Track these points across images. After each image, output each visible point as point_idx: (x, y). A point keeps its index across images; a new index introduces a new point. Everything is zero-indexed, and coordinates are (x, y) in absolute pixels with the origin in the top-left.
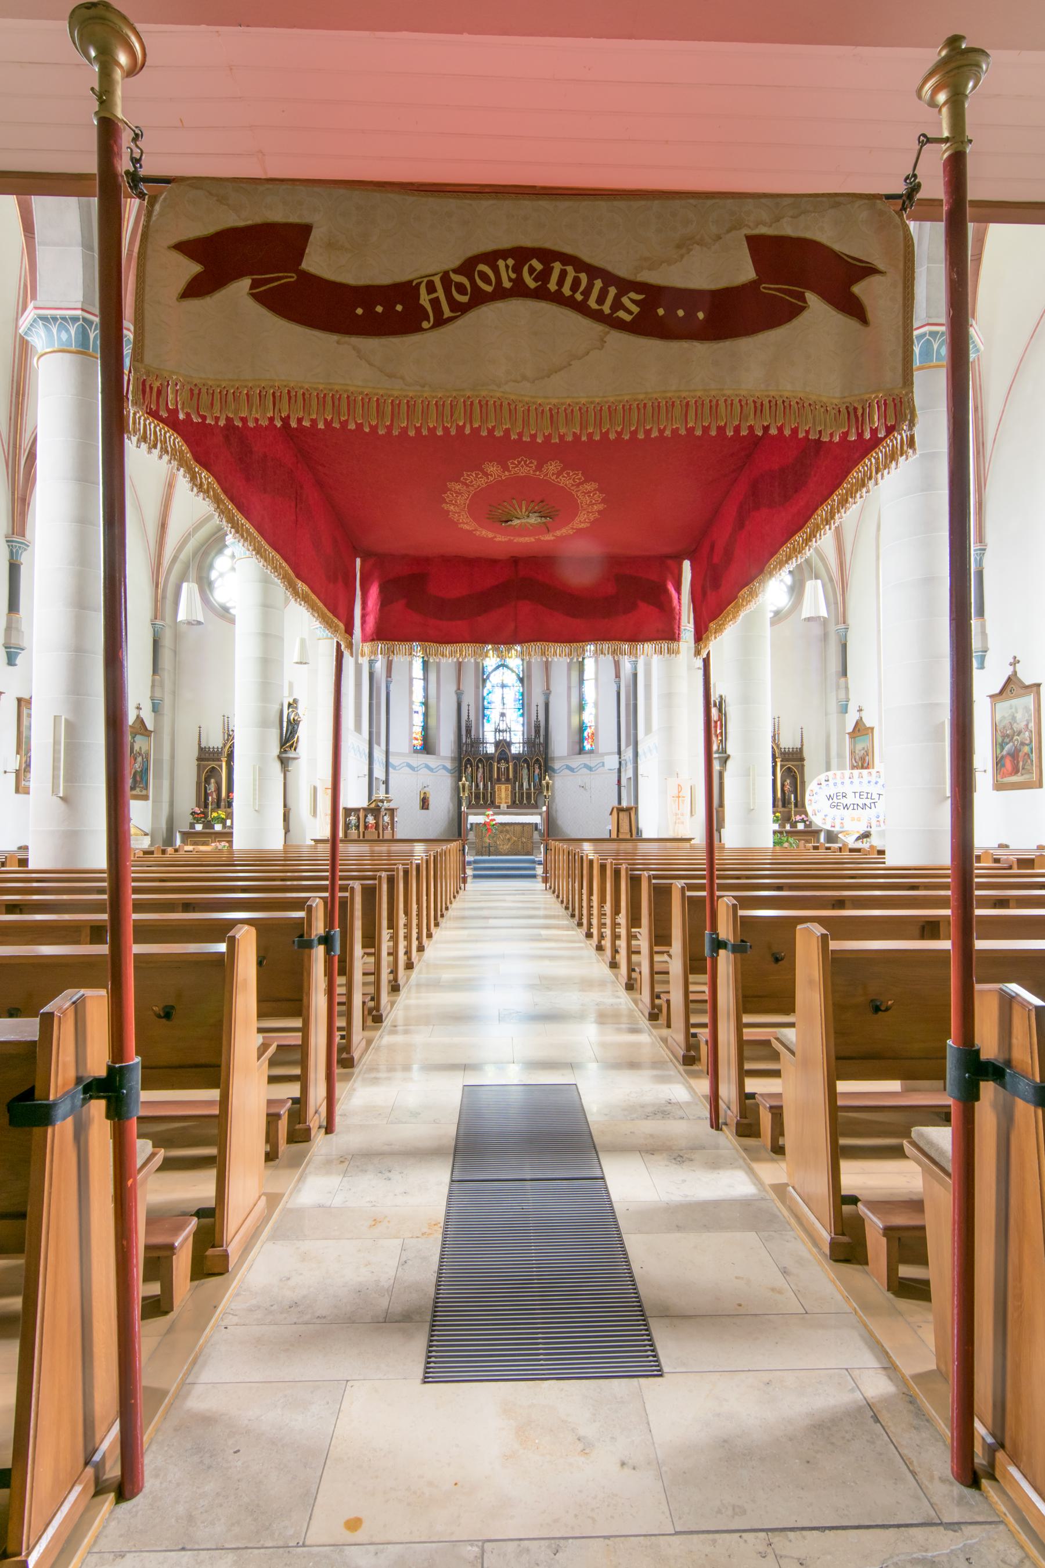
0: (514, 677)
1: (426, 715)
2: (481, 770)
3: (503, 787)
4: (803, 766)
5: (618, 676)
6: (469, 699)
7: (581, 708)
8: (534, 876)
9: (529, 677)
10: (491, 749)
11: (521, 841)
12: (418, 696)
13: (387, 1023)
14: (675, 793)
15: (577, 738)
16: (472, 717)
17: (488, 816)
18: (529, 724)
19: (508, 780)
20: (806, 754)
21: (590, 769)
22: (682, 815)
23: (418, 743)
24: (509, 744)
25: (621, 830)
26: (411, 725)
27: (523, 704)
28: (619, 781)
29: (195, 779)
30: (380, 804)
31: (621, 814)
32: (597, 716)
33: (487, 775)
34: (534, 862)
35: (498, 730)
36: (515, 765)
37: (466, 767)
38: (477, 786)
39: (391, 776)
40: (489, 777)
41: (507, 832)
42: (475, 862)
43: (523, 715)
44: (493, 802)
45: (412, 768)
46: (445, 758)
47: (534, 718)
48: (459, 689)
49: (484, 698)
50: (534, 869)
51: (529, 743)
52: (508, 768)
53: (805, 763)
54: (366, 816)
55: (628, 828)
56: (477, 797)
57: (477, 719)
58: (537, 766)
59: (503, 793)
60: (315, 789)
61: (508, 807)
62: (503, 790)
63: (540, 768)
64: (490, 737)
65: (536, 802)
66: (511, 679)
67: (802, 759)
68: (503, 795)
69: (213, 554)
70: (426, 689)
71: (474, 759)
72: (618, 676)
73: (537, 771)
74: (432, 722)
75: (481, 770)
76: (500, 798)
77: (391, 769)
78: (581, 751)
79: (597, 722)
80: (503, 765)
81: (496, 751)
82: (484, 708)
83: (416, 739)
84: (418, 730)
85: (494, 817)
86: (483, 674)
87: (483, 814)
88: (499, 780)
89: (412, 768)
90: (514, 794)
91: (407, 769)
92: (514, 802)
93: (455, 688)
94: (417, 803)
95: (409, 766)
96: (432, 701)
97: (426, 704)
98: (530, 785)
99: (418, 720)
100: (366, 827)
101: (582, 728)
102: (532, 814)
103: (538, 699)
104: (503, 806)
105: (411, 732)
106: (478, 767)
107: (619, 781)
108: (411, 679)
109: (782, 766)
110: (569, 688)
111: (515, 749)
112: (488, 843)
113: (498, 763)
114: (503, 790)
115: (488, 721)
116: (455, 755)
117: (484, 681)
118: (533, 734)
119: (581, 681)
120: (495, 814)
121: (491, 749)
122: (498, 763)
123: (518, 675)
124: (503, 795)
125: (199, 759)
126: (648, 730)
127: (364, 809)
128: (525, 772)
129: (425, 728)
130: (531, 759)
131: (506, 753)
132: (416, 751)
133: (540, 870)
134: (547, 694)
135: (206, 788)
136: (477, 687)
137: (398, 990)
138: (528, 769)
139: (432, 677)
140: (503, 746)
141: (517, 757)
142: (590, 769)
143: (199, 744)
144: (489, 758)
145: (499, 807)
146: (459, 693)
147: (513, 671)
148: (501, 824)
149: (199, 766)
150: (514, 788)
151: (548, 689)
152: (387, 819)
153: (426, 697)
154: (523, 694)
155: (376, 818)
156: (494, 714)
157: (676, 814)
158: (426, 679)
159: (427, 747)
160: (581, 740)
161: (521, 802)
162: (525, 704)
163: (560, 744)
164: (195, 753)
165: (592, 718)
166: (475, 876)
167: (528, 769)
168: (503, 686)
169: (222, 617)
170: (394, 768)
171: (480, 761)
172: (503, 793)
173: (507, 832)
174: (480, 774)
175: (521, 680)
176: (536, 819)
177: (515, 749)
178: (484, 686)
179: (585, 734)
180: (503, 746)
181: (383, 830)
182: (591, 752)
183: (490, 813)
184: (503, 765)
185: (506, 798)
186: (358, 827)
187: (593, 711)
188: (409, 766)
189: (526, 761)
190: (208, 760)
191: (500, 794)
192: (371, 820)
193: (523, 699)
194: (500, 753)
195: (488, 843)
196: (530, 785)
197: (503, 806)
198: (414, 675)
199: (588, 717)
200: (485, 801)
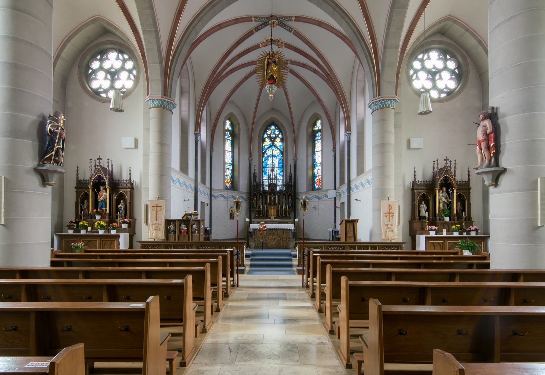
0: (278, 151)
1: (233, 170)
2: (261, 199)
3: (272, 207)
4: (469, 193)
5: (334, 147)
6: (255, 162)
7: (314, 167)
8: (291, 266)
9: (286, 151)
10: (266, 188)
11: (282, 240)
12: (228, 158)
13: (230, 298)
14: (387, 210)
15: (311, 183)
16: (257, 171)
17: (262, 224)
18: (286, 175)
19: (275, 204)
20: (471, 185)
21: (318, 198)
22: (392, 225)
23: (228, 185)
24: (276, 185)
25: (348, 235)
26: (224, 175)
27: (283, 165)
28: (335, 204)
29: (75, 201)
30: (189, 217)
31: (348, 225)
32: (322, 171)
33: (264, 201)
34: (290, 255)
35: (269, 178)
36: (279, 196)
37: (253, 198)
38: (259, 207)
39: (213, 201)
40: (265, 203)
41: (274, 234)
42: (253, 255)
43: (283, 171)
44: (267, 215)
45: (225, 198)
46: (242, 193)
47: (289, 172)
48: (250, 157)
49: (263, 162)
50: (291, 260)
51: (286, 185)
52: (275, 198)
53: (471, 191)
54: (180, 225)
55: (352, 233)
56: (259, 213)
57: (259, 173)
58: (290, 197)
59: (272, 211)
60: (147, 206)
61: (275, 218)
62: (273, 209)
63: (292, 198)
64: (266, 182)
65: (289, 215)
66: (276, 152)
67: (469, 189)
68: (273, 212)
69: (88, 58)
70: (233, 157)
71: (258, 193)
72: (334, 147)
73: (290, 200)
74: (236, 174)
75: (261, 199)
76: (271, 213)
77: (213, 198)
78: (313, 189)
79: (322, 175)
80: (272, 197)
81: (269, 188)
82: (263, 167)
83: (228, 183)
84: (228, 178)
85: (266, 225)
86: (263, 150)
87: (258, 223)
88: (270, 204)
89: (225, 198)
90: (278, 211)
91: (222, 198)
92: (278, 215)
93: (247, 156)
94: (228, 216)
95: (223, 196)
96: (236, 163)
97: (233, 164)
98: (286, 207)
99: (228, 172)
100: (180, 232)
101: (314, 176)
102: (287, 223)
103: (290, 162)
104: (273, 218)
105: (224, 179)
106: (260, 198)
107: (335, 204)
108: (224, 151)
109: (457, 193)
110: (307, 156)
111: (278, 189)
112: (261, 240)
113: (270, 195)
114: (273, 209)
115: (265, 175)
116: (248, 191)
117: (263, 154)
118: (288, 180)
119: (314, 153)
120: (266, 223)
121: (266, 188)
122: (270, 195)
123: (280, 151)
124: (273, 212)
125: (77, 188)
126: (361, 170)
127: (179, 220)
128: (284, 200)
129: (232, 177)
130: (287, 193)
131: (274, 190)
132: (227, 189)
133: (295, 262)
134: (295, 160)
135: (81, 206)
136: (259, 156)
137: (206, 332)
138: (286, 200)
139: (236, 151)
140: (272, 186)
141: (280, 192)
142: (318, 198)
143: (77, 178)
144: (266, 192)
145: (270, 218)
146: (250, 159)
147: (278, 149)
148: (270, 229)
149: (77, 192)
150: (278, 208)
151: (296, 157)
152: (195, 226)
153: (233, 161)
154: (283, 160)
155: (187, 226)
156: (268, 171)
157: (387, 225)
158: (233, 152)
159: (234, 186)
160: (313, 183)
161: (282, 216)
162: (284, 165)
163: (302, 185)
164: (74, 184)
165: (319, 172)
166: (252, 266)
167: (286, 200)
168: (273, 156)
169: (93, 97)
170: (215, 197)
171: (261, 194)
172: (272, 211)
173: (274, 234)
174: (260, 201)
175: (282, 153)
176: (291, 226)
177: (278, 189)
178: (263, 156)
179: (316, 180)
180: (272, 186)
181: (192, 234)
182: (319, 189)
183: (264, 222)
184: (272, 197)
185: (274, 213)
186: (175, 232)
187: (320, 168)
188: (223, 196)
189: (284, 194)
190: (83, 188)
191: (271, 212)
192: (183, 227)
193: (283, 163)
194: (271, 190)
195: (261, 240)
196: (286, 207)
197: (273, 218)
198: (226, 149)
199: (318, 170)
200: (263, 215)
